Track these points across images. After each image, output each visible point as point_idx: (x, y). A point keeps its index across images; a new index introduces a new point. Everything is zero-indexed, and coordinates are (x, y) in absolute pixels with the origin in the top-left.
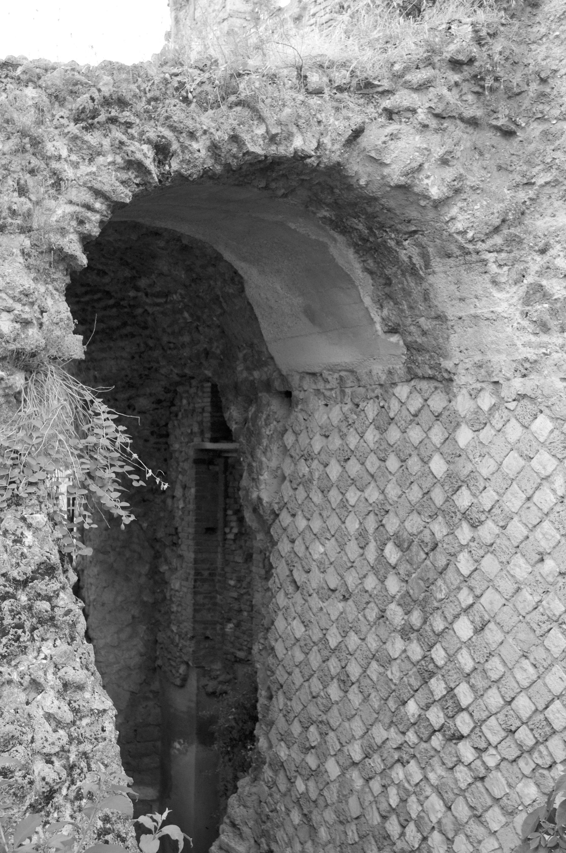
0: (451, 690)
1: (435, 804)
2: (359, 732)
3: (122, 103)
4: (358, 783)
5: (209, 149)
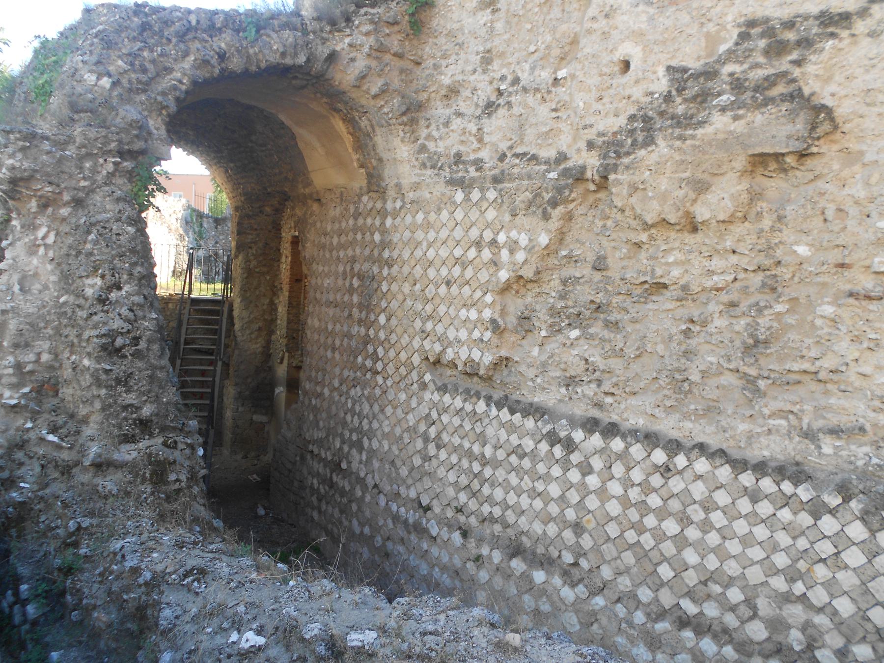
1: (366, 407)
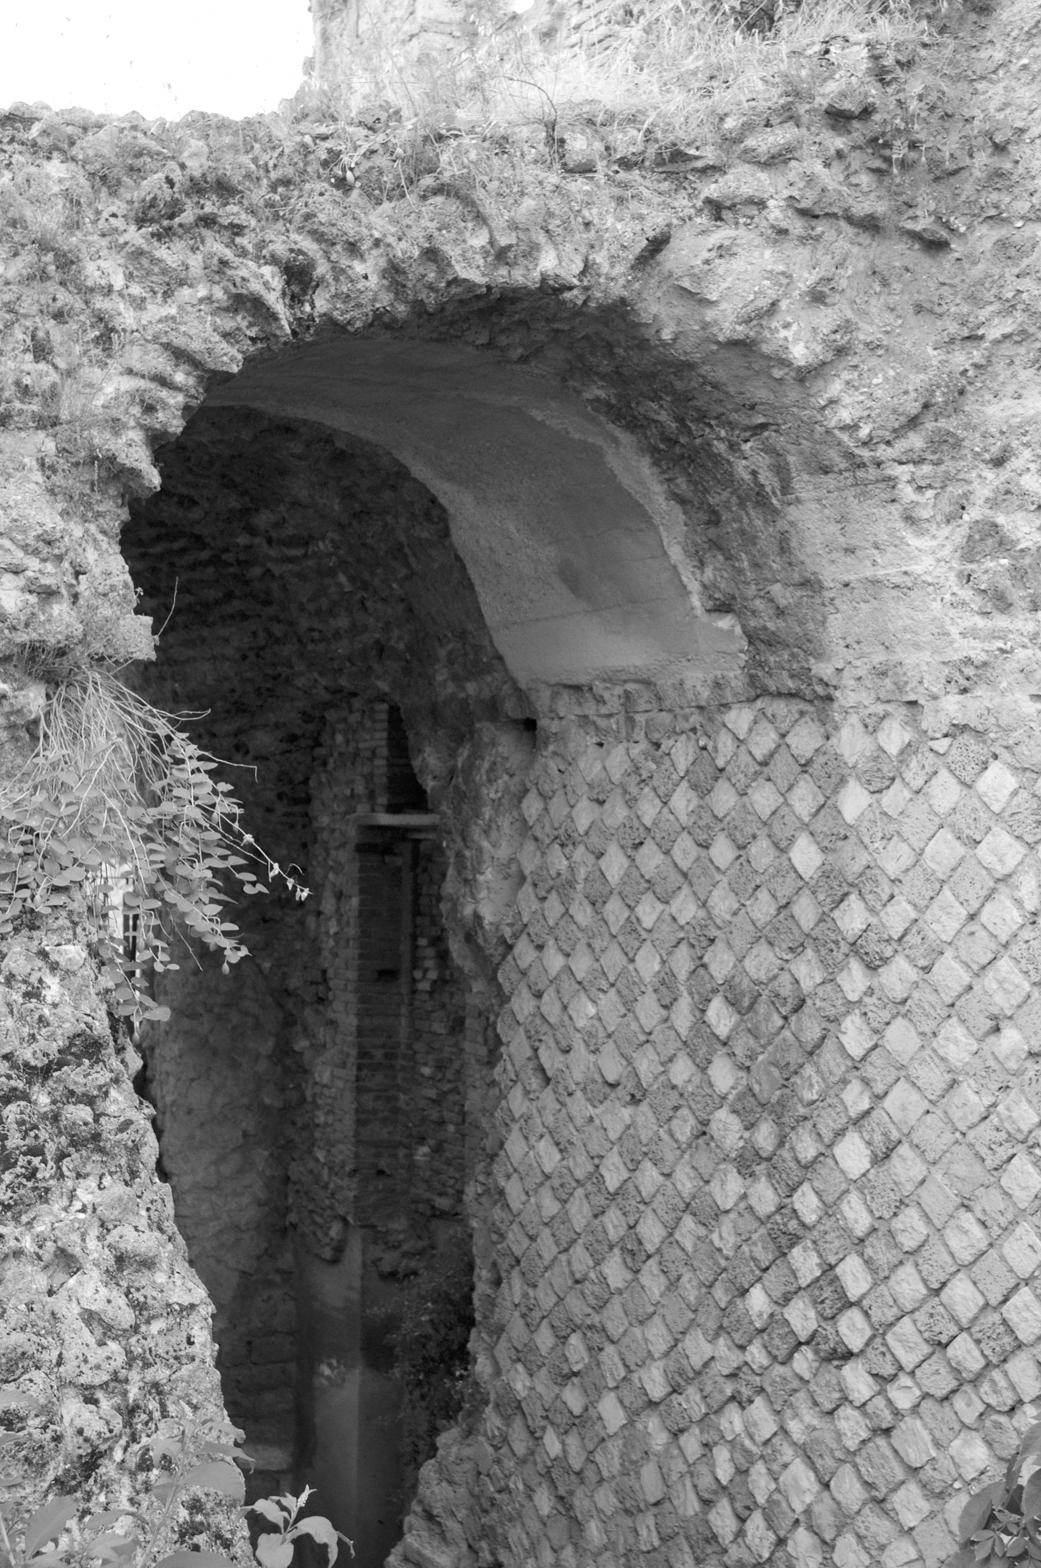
0: (829, 1268)
1: (801, 1478)
2: (659, 1346)
3: (224, 189)
4: (659, 1439)
5: (384, 274)
